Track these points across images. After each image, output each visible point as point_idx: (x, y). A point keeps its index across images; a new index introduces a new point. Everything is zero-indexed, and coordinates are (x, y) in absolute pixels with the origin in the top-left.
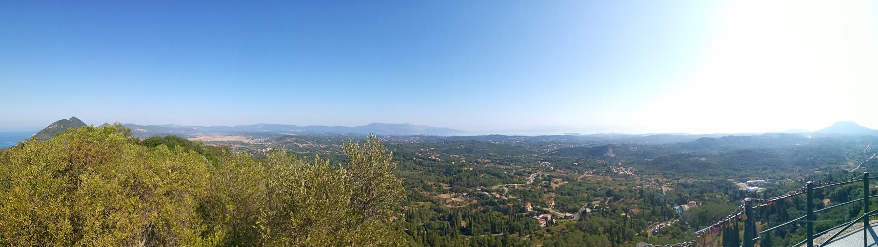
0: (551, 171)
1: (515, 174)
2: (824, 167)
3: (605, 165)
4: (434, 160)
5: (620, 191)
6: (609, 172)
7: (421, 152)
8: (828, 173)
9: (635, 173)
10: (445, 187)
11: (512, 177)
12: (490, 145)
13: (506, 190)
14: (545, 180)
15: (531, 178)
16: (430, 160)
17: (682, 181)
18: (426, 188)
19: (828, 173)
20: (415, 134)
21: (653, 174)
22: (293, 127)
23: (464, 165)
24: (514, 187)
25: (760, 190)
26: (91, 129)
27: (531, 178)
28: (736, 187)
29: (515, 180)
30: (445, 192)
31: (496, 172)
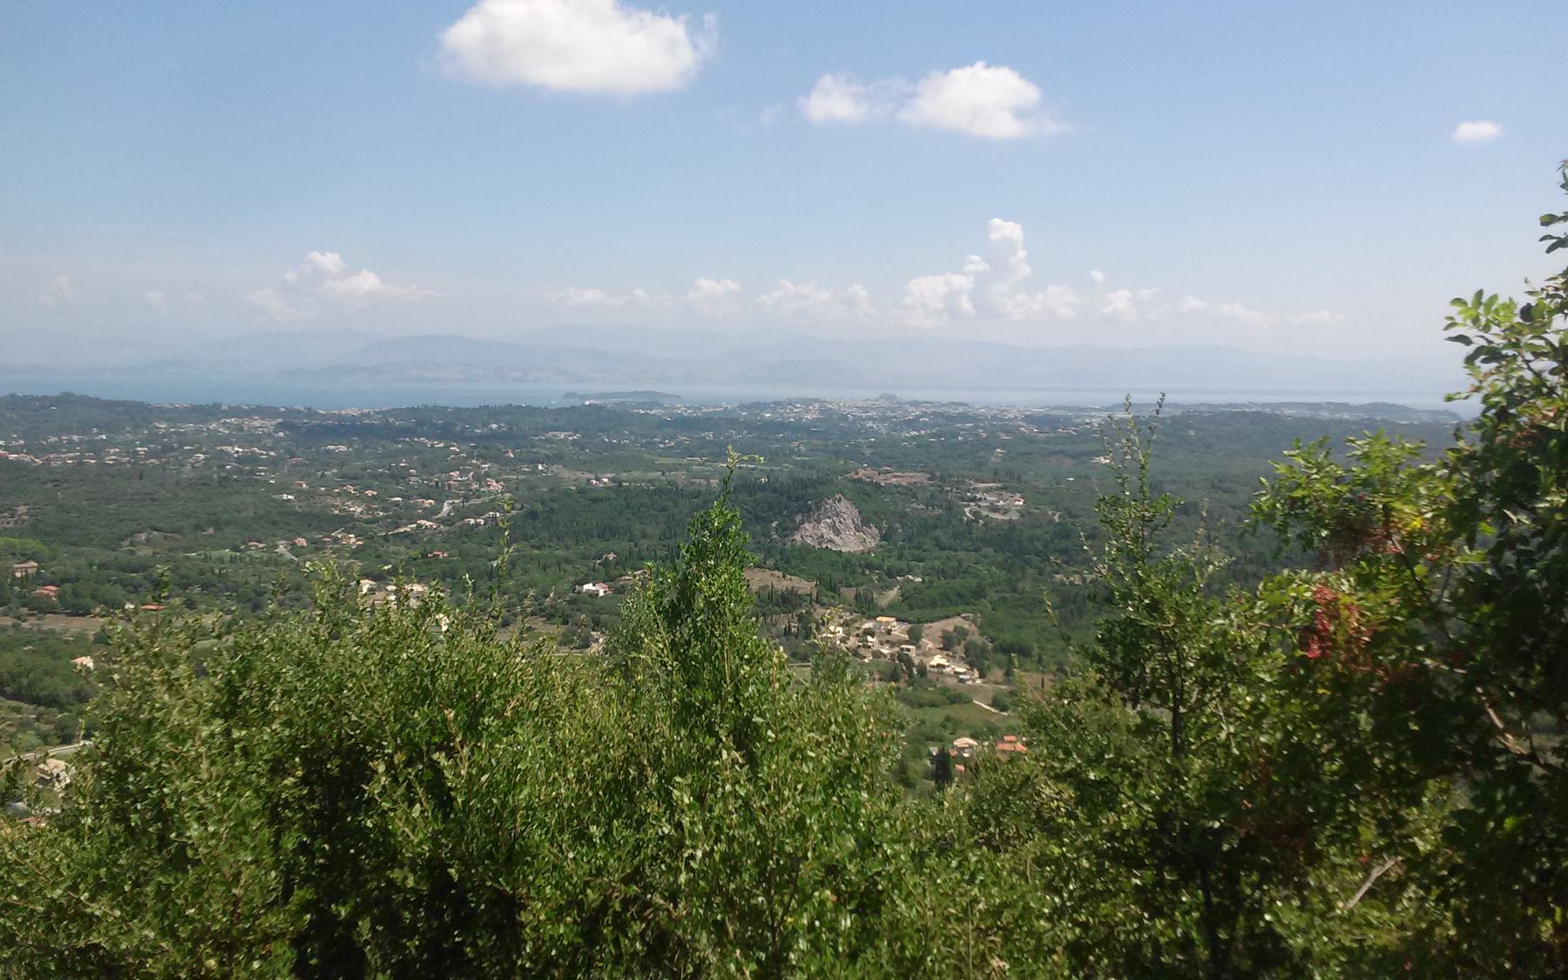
3: (787, 601)
9: (975, 659)
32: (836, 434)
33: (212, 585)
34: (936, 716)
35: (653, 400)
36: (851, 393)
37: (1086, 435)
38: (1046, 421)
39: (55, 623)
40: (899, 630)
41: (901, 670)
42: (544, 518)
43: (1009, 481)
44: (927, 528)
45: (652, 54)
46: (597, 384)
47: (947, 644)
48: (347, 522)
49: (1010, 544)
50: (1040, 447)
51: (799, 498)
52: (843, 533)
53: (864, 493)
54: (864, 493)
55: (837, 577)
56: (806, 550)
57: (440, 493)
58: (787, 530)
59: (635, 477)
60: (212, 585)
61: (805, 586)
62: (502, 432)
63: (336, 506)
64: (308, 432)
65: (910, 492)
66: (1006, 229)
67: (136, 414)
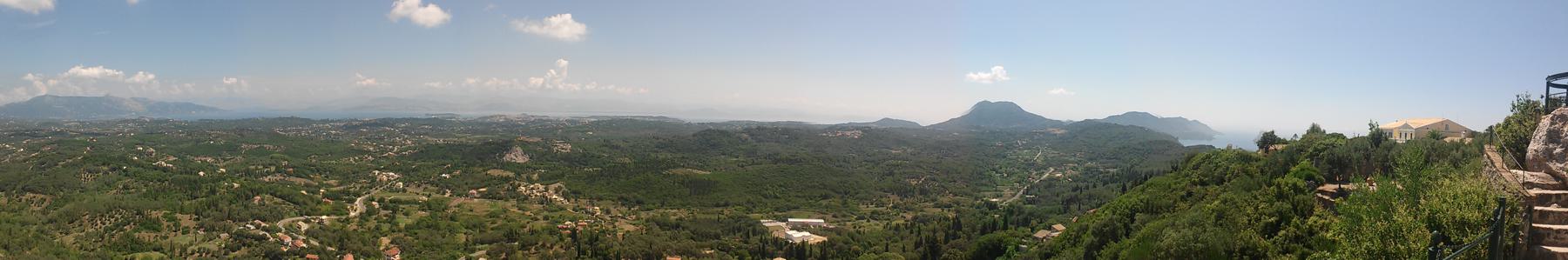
0: (398, 191)
1: (325, 196)
2: (945, 200)
3: (507, 179)
4: (165, 170)
5: (532, 232)
6: (513, 193)
7: (139, 153)
8: (951, 215)
9: (565, 196)
10: (186, 220)
11: (319, 203)
12: (274, 138)
13: (305, 227)
14: (385, 208)
15: (359, 206)
16: (156, 168)
17: (656, 214)
18: (154, 226)
19: (951, 215)
20: (127, 116)
21: (600, 199)
22: (188, 106)
23: (222, 177)
24: (321, 222)
25: (814, 239)
26: (1508, 121)
27: (359, 206)
28: (765, 230)
29: (324, 208)
30: (186, 231)
31: (286, 192)
32: (510, 125)
33: (331, 172)
34: (556, 215)
35: (453, 116)
36: (514, 114)
37: (586, 125)
38: (572, 121)
39: (293, 179)
40: (542, 188)
41: (544, 201)
42: (425, 153)
43: (566, 140)
44: (544, 155)
45: (433, 15)
46: (435, 112)
47: (557, 192)
48: (368, 152)
49: (567, 158)
50: (571, 129)
51: (505, 146)
52: (518, 157)
53: (524, 144)
54: (524, 144)
55: (519, 169)
56: (508, 163)
57: (394, 144)
58: (501, 156)
59: (451, 140)
60: (331, 172)
61: (512, 175)
62: (413, 126)
63: (366, 147)
64: (352, 127)
65: (537, 144)
66: (564, 63)
67: (308, 122)
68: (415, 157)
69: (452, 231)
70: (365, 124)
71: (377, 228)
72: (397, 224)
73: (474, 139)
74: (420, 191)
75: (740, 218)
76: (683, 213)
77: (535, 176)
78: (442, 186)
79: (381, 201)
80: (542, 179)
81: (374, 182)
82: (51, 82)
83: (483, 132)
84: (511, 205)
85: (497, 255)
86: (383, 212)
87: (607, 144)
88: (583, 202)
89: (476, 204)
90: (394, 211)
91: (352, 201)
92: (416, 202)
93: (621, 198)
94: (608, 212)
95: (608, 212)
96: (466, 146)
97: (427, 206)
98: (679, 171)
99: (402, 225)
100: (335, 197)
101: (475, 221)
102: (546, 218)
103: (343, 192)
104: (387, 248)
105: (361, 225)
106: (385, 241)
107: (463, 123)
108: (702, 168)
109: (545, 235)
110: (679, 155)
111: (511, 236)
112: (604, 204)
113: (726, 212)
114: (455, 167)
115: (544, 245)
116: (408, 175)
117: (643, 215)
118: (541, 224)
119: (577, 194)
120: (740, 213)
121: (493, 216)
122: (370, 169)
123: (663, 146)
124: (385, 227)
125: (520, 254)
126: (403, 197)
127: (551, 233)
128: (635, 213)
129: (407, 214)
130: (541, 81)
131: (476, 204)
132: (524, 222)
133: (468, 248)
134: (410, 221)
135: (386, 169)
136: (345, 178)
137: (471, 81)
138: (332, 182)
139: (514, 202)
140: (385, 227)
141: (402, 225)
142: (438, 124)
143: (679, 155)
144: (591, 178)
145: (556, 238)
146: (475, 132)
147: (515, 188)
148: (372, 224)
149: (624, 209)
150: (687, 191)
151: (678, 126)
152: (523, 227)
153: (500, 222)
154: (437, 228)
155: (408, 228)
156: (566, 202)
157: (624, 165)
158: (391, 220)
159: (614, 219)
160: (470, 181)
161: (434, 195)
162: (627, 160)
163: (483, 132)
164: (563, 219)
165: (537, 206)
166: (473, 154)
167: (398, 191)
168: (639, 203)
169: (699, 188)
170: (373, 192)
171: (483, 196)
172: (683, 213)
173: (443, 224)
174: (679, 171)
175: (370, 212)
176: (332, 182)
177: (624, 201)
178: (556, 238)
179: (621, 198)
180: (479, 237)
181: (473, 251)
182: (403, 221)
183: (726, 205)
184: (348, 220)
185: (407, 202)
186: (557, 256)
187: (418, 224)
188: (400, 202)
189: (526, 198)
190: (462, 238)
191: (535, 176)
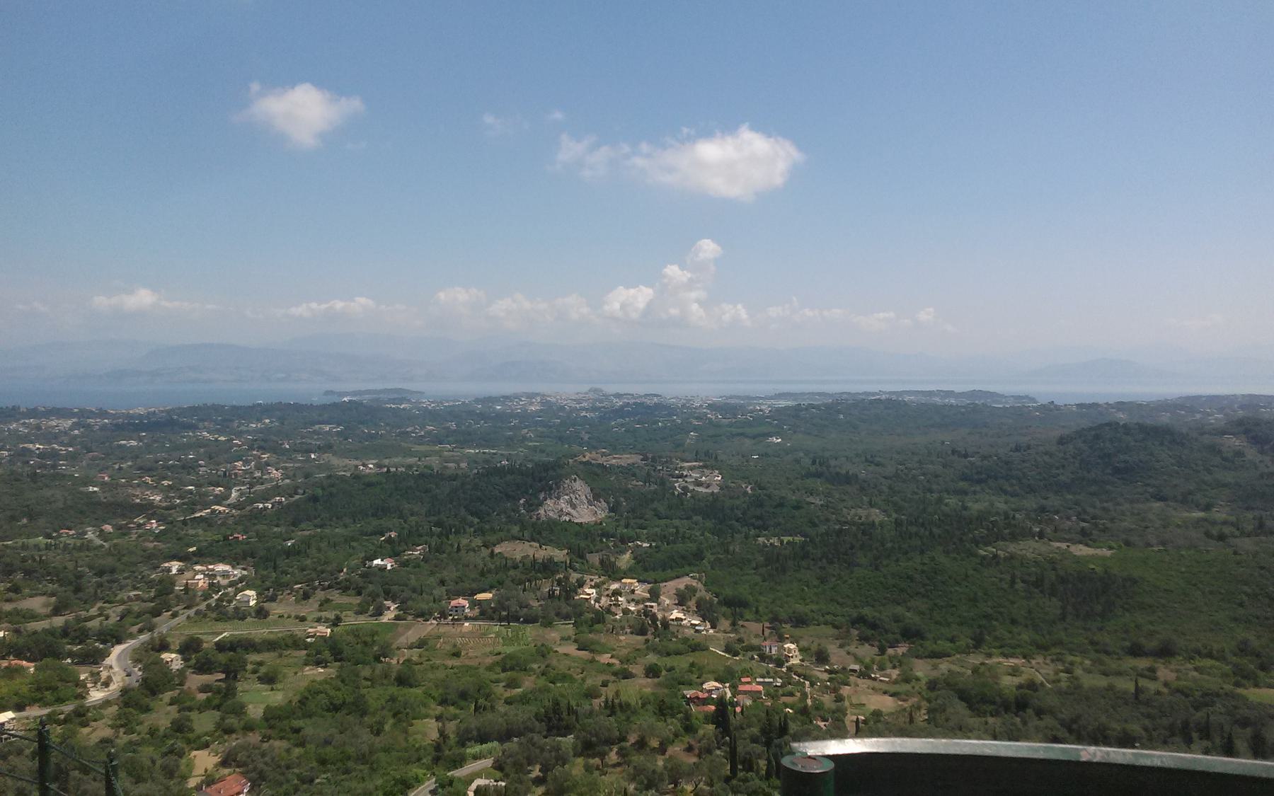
3: (547, 568)
5: (612, 708)
6: (565, 604)
9: (705, 611)
15: (118, 666)
21: (800, 621)
27: (118, 666)
34: (682, 663)
35: (402, 395)
36: (567, 389)
37: (760, 419)
40: (641, 590)
41: (647, 624)
43: (709, 461)
46: (353, 385)
47: (681, 600)
48: (148, 509)
49: (711, 509)
50: (725, 429)
51: (543, 479)
52: (578, 507)
53: (593, 474)
54: (593, 474)
55: (584, 542)
57: (227, 481)
58: (533, 506)
59: (397, 463)
61: (559, 555)
62: (286, 425)
65: (629, 471)
68: (293, 516)
69: (403, 714)
70: (130, 425)
71: (179, 727)
72: (239, 710)
73: (463, 459)
74: (310, 609)
75: (1209, 698)
76: (1040, 670)
77: (625, 560)
78: (371, 591)
79: (189, 648)
80: (643, 568)
81: (165, 596)
82: (808, 313)
83: (486, 441)
84: (560, 640)
85: (520, 768)
86: (196, 681)
87: (821, 470)
88: (753, 629)
89: (468, 635)
90: (232, 673)
91: (94, 658)
92: (296, 643)
93: (860, 621)
94: (822, 658)
95: (822, 658)
96: (439, 477)
97: (331, 651)
98: (1028, 549)
99: (255, 711)
100: (43, 649)
101: (466, 682)
102: (652, 672)
103: (65, 632)
104: (210, 780)
105: (124, 723)
106: (204, 760)
107: (431, 415)
108: (1085, 537)
109: (646, 720)
110: (1031, 503)
111: (556, 720)
112: (812, 636)
113: (1165, 673)
114: (409, 539)
115: (641, 744)
116: (272, 568)
117: (922, 669)
118: (638, 688)
119: (736, 607)
120: (1212, 683)
121: (511, 665)
122: (154, 559)
123: (985, 475)
124: (204, 722)
125: (577, 768)
126: (259, 632)
127: (663, 710)
128: (897, 662)
129: (270, 680)
130: (642, 296)
131: (468, 635)
132: (593, 681)
133: (443, 757)
134: (277, 698)
135: (205, 555)
136: (72, 590)
137: (461, 295)
138: (36, 604)
139: (568, 629)
140: (204, 722)
141: (255, 711)
142: (359, 419)
143: (1031, 503)
144: (775, 563)
145: (674, 724)
146: (465, 438)
147: (569, 591)
148: (162, 715)
149: (867, 651)
150: (1052, 606)
151: (1024, 414)
152: (591, 694)
153: (528, 683)
154: (359, 708)
155: (273, 717)
156: (707, 630)
157: (867, 529)
158: (223, 699)
159: (839, 678)
160: (450, 573)
161: (352, 620)
162: (877, 515)
163: (486, 441)
164: (698, 673)
165: (627, 640)
166: (446, 498)
167: (240, 615)
168: (910, 634)
169: (1088, 600)
170: (164, 625)
171: (486, 613)
172: (1040, 670)
173: (375, 696)
174: (1028, 549)
175: (154, 683)
176: (36, 604)
177: (870, 630)
178: (674, 724)
179: (860, 621)
180: (474, 723)
181: (458, 762)
182: (257, 700)
183: (1165, 652)
184: (82, 716)
185: (271, 645)
186: (675, 775)
187: (304, 704)
188: (250, 646)
189: (599, 618)
190: (428, 730)
191: (625, 560)
